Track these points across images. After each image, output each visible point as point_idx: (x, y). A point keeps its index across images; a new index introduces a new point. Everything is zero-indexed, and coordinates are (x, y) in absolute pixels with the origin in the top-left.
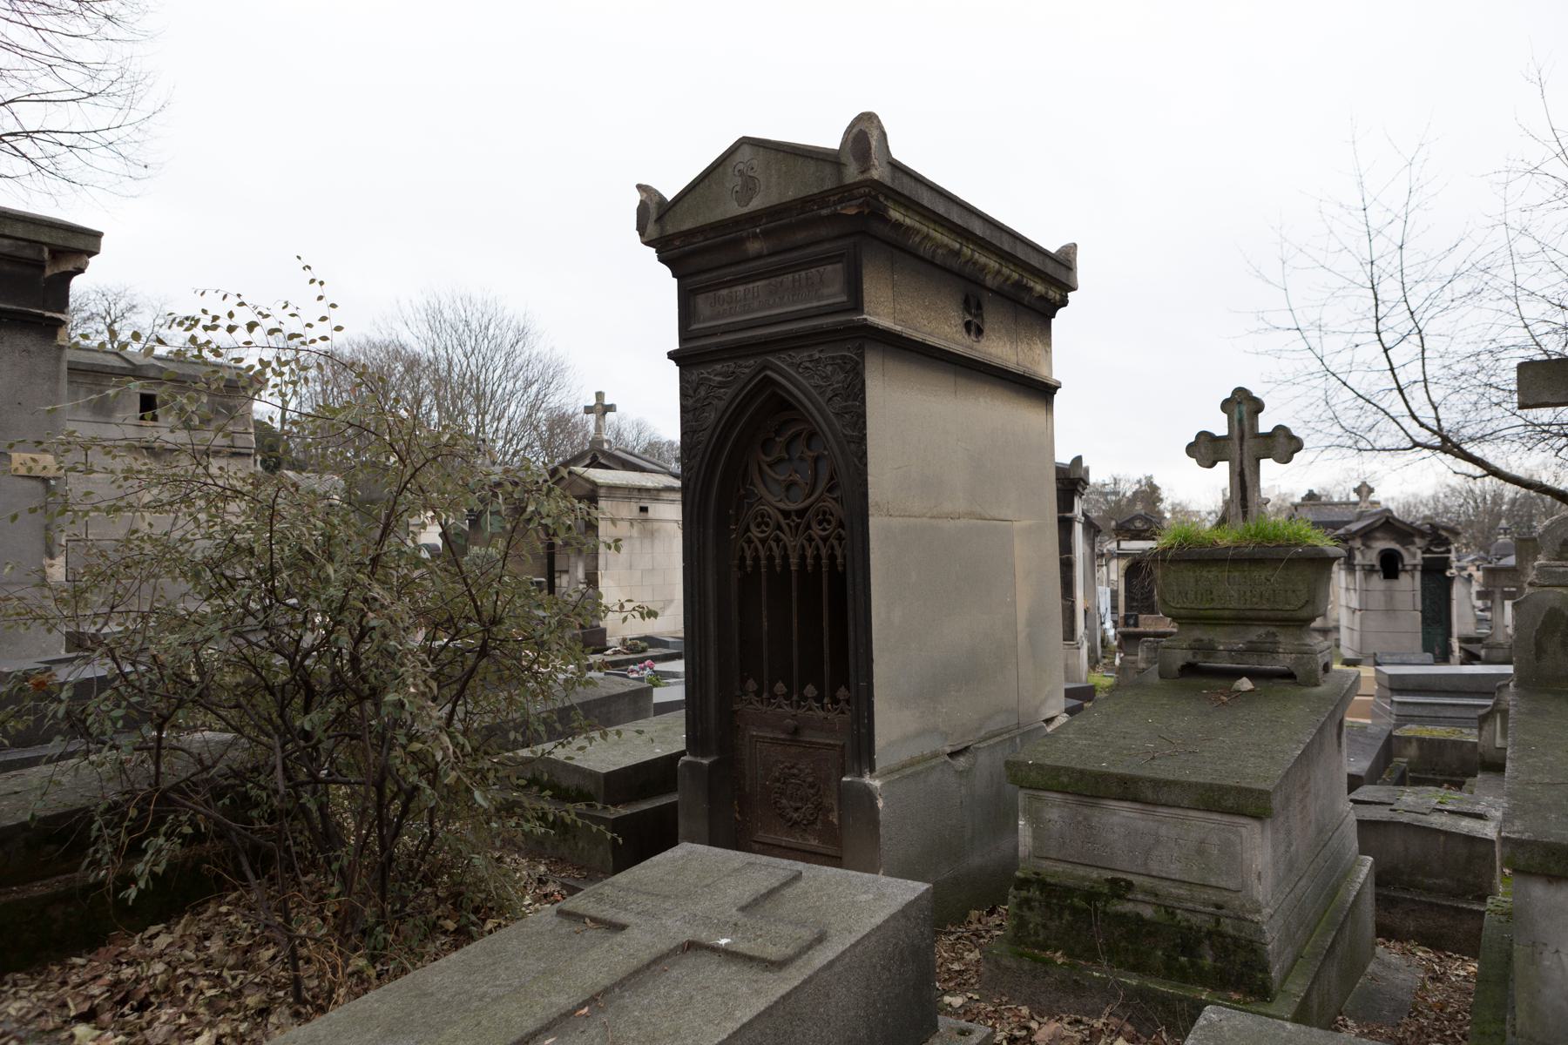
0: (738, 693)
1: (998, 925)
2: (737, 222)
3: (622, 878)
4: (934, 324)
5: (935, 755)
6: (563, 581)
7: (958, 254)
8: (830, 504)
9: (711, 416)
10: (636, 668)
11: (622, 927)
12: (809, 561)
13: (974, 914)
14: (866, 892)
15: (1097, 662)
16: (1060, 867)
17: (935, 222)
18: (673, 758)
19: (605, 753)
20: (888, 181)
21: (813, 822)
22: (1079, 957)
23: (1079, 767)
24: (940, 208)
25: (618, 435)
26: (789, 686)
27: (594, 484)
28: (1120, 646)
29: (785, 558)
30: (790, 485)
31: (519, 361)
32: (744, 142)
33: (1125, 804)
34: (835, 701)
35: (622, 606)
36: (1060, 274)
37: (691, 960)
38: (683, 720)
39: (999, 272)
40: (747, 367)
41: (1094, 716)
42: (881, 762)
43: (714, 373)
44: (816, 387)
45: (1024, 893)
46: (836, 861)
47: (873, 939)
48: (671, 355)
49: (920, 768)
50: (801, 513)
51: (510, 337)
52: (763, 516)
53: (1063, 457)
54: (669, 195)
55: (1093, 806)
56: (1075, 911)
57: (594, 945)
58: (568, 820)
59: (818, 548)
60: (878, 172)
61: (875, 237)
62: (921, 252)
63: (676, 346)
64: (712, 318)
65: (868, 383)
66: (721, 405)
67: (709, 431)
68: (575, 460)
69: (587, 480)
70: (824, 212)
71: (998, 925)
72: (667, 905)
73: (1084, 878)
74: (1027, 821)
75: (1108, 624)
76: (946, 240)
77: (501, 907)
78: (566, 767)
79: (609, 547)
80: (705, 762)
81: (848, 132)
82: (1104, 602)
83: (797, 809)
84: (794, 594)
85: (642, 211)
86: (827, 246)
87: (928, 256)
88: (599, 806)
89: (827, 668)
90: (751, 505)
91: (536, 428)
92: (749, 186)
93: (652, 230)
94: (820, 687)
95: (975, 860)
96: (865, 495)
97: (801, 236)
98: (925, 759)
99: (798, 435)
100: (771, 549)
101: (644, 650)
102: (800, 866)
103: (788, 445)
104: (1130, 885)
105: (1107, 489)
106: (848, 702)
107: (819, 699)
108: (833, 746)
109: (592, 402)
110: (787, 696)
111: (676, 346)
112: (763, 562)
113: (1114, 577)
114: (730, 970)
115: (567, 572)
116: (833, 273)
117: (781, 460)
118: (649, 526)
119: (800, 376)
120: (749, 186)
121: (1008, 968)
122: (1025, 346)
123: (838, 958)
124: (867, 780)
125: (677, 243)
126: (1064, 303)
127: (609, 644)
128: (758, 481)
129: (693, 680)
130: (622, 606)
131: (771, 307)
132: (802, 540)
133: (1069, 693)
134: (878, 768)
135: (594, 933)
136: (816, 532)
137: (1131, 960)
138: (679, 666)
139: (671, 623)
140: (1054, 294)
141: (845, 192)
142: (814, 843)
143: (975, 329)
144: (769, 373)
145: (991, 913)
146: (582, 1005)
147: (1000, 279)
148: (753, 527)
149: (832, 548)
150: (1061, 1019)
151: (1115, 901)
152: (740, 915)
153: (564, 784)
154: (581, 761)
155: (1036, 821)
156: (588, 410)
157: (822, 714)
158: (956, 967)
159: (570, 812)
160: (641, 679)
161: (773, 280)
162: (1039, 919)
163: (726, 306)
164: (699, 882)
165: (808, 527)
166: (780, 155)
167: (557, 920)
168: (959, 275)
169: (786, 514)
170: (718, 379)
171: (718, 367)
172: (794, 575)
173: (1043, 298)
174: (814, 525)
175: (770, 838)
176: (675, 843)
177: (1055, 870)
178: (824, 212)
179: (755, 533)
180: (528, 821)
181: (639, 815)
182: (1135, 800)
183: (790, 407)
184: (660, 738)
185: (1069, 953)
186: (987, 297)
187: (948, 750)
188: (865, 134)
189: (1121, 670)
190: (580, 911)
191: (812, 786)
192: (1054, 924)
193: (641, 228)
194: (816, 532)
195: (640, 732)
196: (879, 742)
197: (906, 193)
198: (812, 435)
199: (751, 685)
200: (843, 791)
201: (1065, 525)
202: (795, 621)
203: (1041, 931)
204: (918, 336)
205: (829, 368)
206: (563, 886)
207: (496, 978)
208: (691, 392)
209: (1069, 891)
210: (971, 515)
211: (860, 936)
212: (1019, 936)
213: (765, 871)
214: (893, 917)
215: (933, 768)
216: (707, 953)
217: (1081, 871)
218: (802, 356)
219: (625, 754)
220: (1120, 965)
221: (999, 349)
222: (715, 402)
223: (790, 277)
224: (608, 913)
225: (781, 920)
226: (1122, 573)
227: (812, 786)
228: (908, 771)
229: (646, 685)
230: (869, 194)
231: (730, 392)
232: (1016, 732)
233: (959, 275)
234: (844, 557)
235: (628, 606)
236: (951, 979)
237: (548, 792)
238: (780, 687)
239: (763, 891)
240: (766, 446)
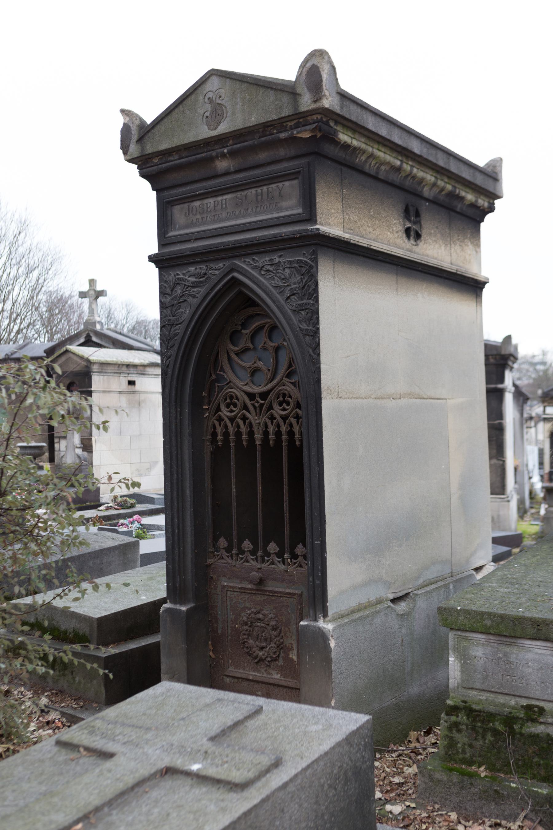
0: (211, 549)
1: (431, 744)
2: (208, 143)
3: (112, 712)
4: (378, 232)
5: (380, 601)
6: (61, 446)
7: (398, 170)
8: (289, 388)
9: (186, 312)
10: (126, 521)
11: (108, 756)
12: (271, 436)
13: (413, 735)
14: (316, 723)
15: (525, 512)
16: (484, 696)
17: (379, 143)
18: (157, 604)
19: (100, 600)
20: (337, 108)
21: (276, 659)
22: (499, 771)
23: (500, 612)
24: (383, 131)
25: (109, 316)
26: (255, 543)
27: (88, 361)
28: (544, 498)
29: (251, 433)
30: (255, 371)
31: (21, 250)
32: (213, 73)
33: (538, 643)
34: (294, 556)
35: (110, 478)
36: (488, 185)
37: (168, 783)
38: (164, 572)
39: (434, 185)
40: (217, 269)
41: (515, 568)
42: (333, 607)
43: (188, 274)
44: (276, 287)
45: (453, 718)
46: (293, 693)
47: (322, 763)
48: (152, 259)
49: (366, 612)
50: (264, 395)
51: (13, 229)
52: (231, 398)
53: (494, 334)
54: (149, 119)
55: (512, 644)
56: (496, 733)
57: (87, 771)
58: (66, 659)
59: (278, 426)
60: (329, 101)
61: (326, 157)
62: (367, 169)
63: (156, 251)
64: (187, 226)
65: (321, 284)
66: (195, 302)
67: (184, 325)
68: (71, 339)
69: (82, 358)
70: (283, 135)
71: (431, 744)
72: (149, 736)
73: (503, 705)
74: (457, 657)
75: (536, 479)
76: (388, 158)
77: (9, 734)
78: (65, 612)
79: (98, 428)
80: (184, 608)
81: (303, 66)
82: (532, 460)
83: (262, 648)
84: (259, 465)
85: (126, 132)
86: (285, 165)
87: (373, 172)
88: (92, 647)
89: (287, 529)
90: (221, 388)
91: (37, 309)
92: (217, 113)
93: (134, 150)
94: (281, 545)
95: (414, 690)
96: (318, 381)
97: (262, 156)
98: (370, 605)
99: (260, 328)
100: (238, 426)
101: (132, 506)
102: (261, 701)
103: (253, 337)
104: (542, 711)
105: (536, 360)
106: (305, 557)
107: (280, 555)
108: (293, 594)
109: (85, 288)
110: (253, 552)
111: (156, 251)
112: (232, 437)
113: (541, 437)
114: (200, 791)
115: (65, 438)
116: (291, 188)
117: (246, 350)
118: (137, 396)
119: (262, 278)
120: (217, 113)
121: (439, 781)
122: (457, 247)
123: (292, 780)
124: (321, 623)
125: (156, 161)
126: (491, 209)
127: (102, 500)
128: (227, 367)
129: (173, 533)
130: (110, 478)
131: (237, 217)
132: (265, 418)
133: (496, 541)
134: (330, 613)
135: (87, 761)
136: (277, 411)
137: (543, 773)
138: (160, 520)
139: (154, 483)
140: (482, 202)
141: (300, 118)
142: (276, 676)
143: (413, 234)
144: (236, 274)
145: (428, 733)
146: (77, 822)
147: (436, 190)
148: (223, 407)
149: (291, 425)
150: (484, 823)
151: (529, 724)
152: (210, 744)
153: (63, 628)
154: (76, 608)
155: (464, 658)
156: (83, 295)
157: (282, 567)
158: (397, 780)
159: (68, 653)
160: (128, 534)
161: (239, 194)
162: (466, 740)
163: (198, 216)
164: (177, 713)
165: (271, 407)
166: (244, 86)
167: (56, 749)
168: (400, 188)
169: (252, 396)
170: (192, 279)
171: (192, 269)
172: (259, 448)
173: (473, 206)
174: (276, 406)
175: (240, 673)
176: (157, 680)
177: (480, 699)
178: (283, 135)
179: (225, 412)
180: (31, 662)
181: (127, 658)
182: (546, 640)
183: (254, 304)
184: (145, 586)
185: (491, 768)
186: (424, 206)
187: (391, 597)
188: (316, 68)
189: (545, 519)
190: (76, 741)
191: (274, 628)
192: (478, 744)
193: (125, 148)
194: (277, 411)
195: (126, 585)
196: (332, 591)
197: (353, 118)
198: (273, 328)
199: (223, 542)
200: (301, 633)
201: (495, 396)
202: (259, 488)
203: (468, 750)
204: (364, 242)
205: (288, 271)
206: (63, 714)
207: (5, 799)
208: (168, 291)
209: (491, 716)
210: (411, 395)
211: (309, 761)
212: (450, 754)
213: (230, 705)
214: (339, 744)
215: (378, 612)
216: (182, 777)
217: (501, 699)
218: (264, 260)
219: (115, 601)
220: (533, 777)
221: (435, 250)
222: (190, 299)
223: (253, 191)
224: (98, 743)
225: (243, 748)
226: (547, 434)
227: (274, 628)
228: (356, 616)
229: (133, 539)
230: (321, 121)
231: (202, 291)
232: (449, 580)
233: (400, 188)
234: (301, 434)
235: (116, 478)
236: (392, 791)
237: (47, 637)
238: (247, 545)
239: (230, 723)
240: (234, 337)
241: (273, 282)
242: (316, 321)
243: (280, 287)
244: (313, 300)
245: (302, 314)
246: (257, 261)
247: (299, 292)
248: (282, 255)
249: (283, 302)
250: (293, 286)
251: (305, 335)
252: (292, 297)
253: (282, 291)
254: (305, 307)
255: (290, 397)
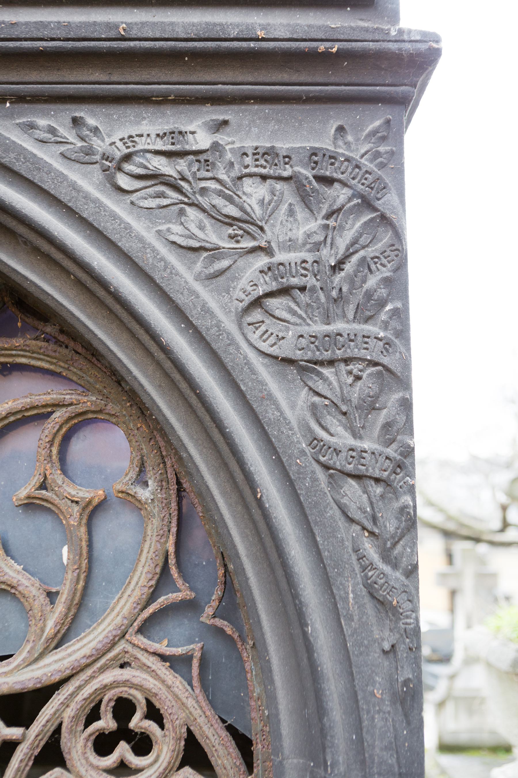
241: (177, 228)
242: (402, 419)
243: (214, 252)
244: (385, 326)
245: (325, 379)
246: (96, 130)
247: (310, 281)
248: (225, 123)
249: (230, 325)
250: (280, 257)
251: (336, 474)
252: (273, 303)
253: (222, 272)
254: (349, 354)
255: (154, 714)
